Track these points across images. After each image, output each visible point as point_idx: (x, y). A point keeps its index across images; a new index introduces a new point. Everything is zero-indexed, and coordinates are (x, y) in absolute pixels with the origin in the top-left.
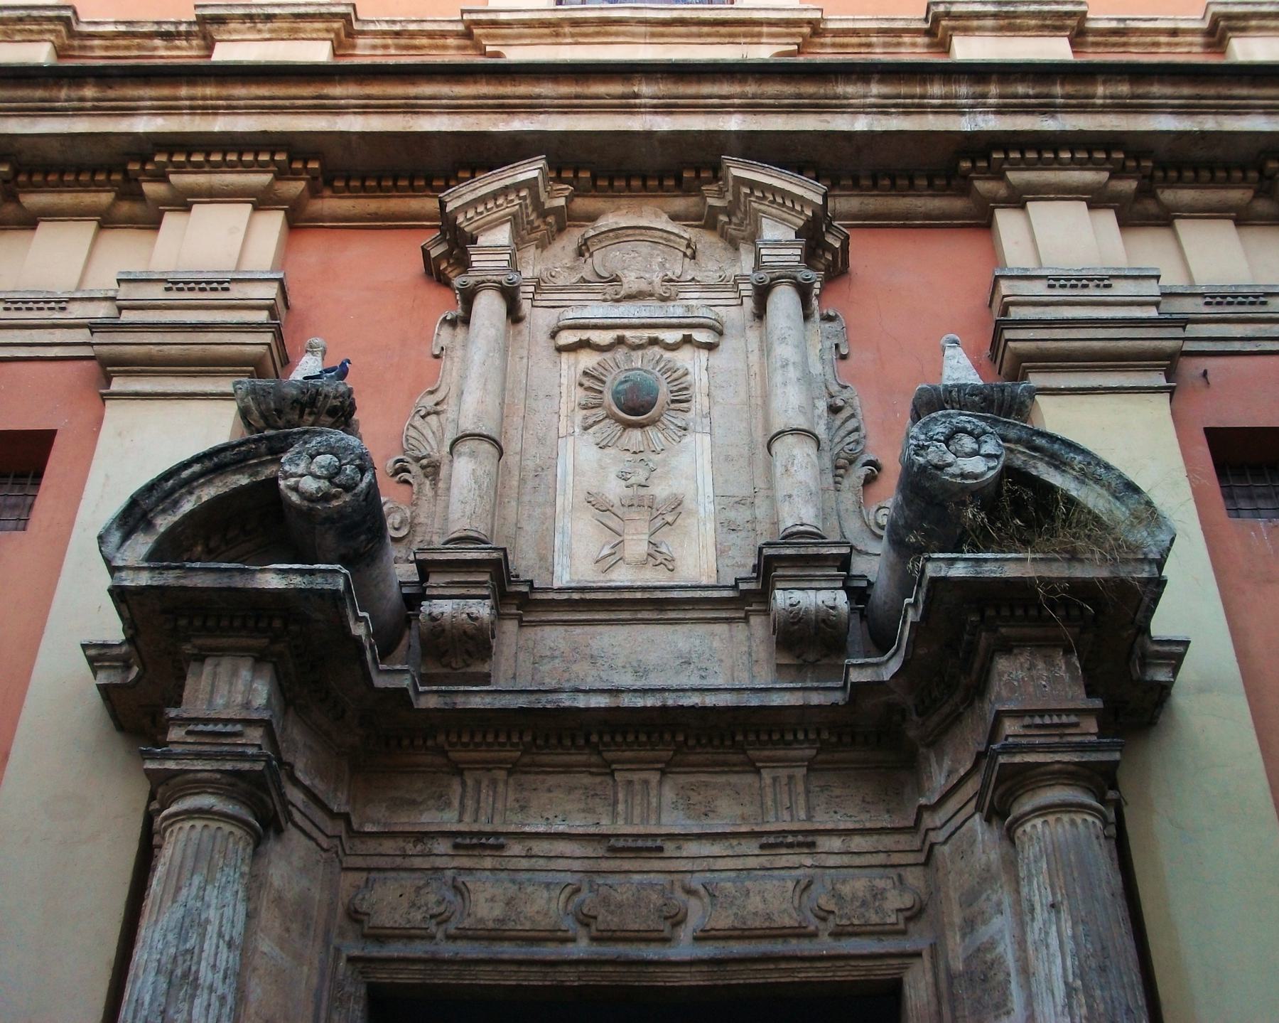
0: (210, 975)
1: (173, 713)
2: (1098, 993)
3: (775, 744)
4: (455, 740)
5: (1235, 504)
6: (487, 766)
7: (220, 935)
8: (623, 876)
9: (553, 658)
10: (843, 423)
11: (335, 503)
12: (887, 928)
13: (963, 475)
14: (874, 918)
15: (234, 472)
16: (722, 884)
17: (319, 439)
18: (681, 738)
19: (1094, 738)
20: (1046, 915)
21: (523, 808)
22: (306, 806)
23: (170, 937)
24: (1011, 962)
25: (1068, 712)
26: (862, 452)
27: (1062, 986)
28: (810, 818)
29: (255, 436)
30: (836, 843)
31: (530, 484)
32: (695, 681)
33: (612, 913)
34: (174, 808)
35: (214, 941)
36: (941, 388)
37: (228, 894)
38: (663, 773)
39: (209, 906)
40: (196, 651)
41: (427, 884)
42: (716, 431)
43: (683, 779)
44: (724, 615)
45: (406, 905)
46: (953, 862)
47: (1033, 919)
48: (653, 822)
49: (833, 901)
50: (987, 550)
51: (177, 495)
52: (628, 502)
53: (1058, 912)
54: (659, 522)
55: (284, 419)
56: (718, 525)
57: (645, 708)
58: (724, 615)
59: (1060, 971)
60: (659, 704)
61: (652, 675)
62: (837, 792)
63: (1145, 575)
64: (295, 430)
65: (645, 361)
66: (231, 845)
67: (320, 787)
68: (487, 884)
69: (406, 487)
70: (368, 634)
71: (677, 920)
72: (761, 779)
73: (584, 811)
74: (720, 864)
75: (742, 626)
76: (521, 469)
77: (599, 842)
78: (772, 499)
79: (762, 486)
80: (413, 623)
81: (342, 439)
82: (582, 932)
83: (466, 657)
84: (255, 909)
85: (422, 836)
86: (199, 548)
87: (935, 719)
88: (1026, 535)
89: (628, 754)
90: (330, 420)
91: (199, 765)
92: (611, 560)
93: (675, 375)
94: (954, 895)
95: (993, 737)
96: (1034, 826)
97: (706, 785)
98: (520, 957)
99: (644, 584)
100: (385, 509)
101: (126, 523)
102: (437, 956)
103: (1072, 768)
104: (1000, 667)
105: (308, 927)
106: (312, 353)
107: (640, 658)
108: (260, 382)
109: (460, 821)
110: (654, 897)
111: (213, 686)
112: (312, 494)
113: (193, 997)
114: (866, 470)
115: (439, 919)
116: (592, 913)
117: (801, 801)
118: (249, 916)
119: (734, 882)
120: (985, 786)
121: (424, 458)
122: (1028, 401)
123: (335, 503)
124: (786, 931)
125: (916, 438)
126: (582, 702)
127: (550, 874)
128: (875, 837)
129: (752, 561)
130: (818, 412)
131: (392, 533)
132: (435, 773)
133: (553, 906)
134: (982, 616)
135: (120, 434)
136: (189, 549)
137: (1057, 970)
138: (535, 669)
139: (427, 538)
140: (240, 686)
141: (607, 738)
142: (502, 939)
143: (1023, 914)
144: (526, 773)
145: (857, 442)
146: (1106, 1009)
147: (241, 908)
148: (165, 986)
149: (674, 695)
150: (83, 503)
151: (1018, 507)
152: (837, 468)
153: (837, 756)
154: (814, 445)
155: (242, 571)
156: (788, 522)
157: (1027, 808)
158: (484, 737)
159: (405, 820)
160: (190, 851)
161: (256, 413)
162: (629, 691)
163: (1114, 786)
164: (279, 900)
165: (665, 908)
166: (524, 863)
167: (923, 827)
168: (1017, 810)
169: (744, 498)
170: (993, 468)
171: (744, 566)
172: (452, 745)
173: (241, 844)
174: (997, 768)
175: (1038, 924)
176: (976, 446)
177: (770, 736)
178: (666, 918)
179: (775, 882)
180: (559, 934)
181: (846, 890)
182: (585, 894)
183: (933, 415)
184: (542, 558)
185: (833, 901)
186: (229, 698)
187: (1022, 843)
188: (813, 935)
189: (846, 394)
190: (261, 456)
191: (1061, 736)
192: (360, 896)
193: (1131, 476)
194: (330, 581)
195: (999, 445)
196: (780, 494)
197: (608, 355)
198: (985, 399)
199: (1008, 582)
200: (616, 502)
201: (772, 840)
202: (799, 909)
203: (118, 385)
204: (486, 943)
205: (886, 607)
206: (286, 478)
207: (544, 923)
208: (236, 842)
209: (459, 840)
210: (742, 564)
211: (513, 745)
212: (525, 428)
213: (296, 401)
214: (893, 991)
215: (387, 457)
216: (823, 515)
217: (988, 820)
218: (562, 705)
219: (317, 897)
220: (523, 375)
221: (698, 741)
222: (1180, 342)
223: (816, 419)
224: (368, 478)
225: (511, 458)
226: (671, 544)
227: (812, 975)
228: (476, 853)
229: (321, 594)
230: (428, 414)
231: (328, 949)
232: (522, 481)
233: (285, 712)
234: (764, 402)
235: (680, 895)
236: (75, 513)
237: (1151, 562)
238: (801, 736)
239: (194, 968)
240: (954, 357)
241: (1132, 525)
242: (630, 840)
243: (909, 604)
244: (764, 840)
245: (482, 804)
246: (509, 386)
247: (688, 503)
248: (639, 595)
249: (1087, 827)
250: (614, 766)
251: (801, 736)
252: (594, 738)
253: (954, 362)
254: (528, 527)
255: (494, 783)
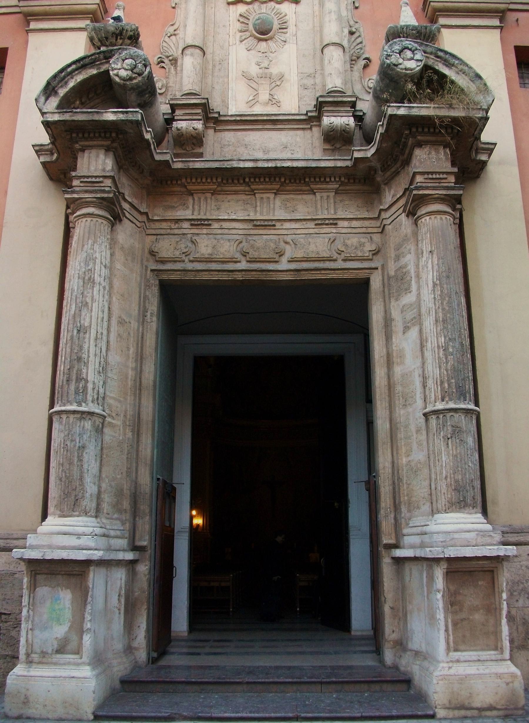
0: (99, 279)
1: (73, 174)
2: (445, 286)
3: (322, 183)
4: (189, 181)
5: (524, 81)
6: (203, 191)
7: (101, 263)
8: (259, 236)
9: (229, 145)
10: (355, 40)
11: (135, 81)
12: (365, 258)
13: (406, 69)
14: (360, 254)
15: (90, 68)
16: (299, 240)
17: (126, 52)
18: (283, 180)
19: (453, 185)
20: (428, 255)
21: (218, 209)
22: (131, 210)
23: (82, 264)
24: (413, 274)
25: (443, 173)
26: (363, 53)
27: (432, 283)
28: (335, 213)
29: (98, 51)
30: (346, 224)
31: (217, 68)
32: (289, 155)
33: (255, 251)
34: (78, 213)
35: (99, 265)
36: (399, 26)
37: (103, 247)
38: (276, 194)
39: (96, 252)
40: (81, 147)
41: (181, 240)
42: (299, 43)
43: (284, 197)
44: (301, 126)
45: (172, 249)
46: (392, 232)
47: (422, 257)
48: (271, 214)
49: (344, 247)
50: (415, 102)
51: (66, 79)
52: (260, 76)
53: (433, 254)
54: (274, 85)
55: (109, 41)
56: (299, 86)
57: (268, 168)
58: (301, 126)
59: (431, 277)
60: (274, 166)
61: (271, 153)
62: (347, 202)
63: (480, 115)
64: (115, 48)
65: (267, 9)
66: (102, 228)
67: (135, 202)
68: (205, 240)
69: (163, 69)
70: (152, 138)
71: (281, 254)
72: (316, 197)
73: (243, 210)
74: (299, 232)
75: (309, 131)
76: (213, 60)
77: (250, 222)
78: (323, 75)
79: (319, 68)
80: (170, 131)
81: (136, 52)
82: (243, 259)
83: (193, 146)
84: (114, 252)
85: (177, 221)
86: (78, 102)
87: (389, 173)
88: (432, 95)
89: (261, 186)
90: (129, 42)
91: (87, 195)
92: (253, 102)
93: (281, 16)
94: (392, 246)
95: (411, 183)
96: (426, 220)
97: (293, 199)
98: (219, 269)
99: (268, 113)
100: (155, 79)
101: (46, 93)
102: (186, 269)
103: (442, 196)
104: (416, 153)
105: (134, 258)
106: (119, 9)
107: (266, 145)
108: (97, 25)
109: (193, 214)
110: (272, 245)
111: (89, 162)
112: (124, 78)
113: (93, 287)
114: (364, 62)
115: (186, 254)
116: (247, 251)
117: (332, 206)
118: (112, 255)
119: (304, 239)
120: (407, 202)
121: (170, 56)
122: (437, 34)
123: (135, 81)
124: (325, 258)
125: (386, 51)
126: (242, 165)
127: (230, 235)
128: (362, 221)
129: (314, 103)
130: (344, 34)
131: (159, 91)
132: (182, 195)
133: (232, 248)
134: (410, 131)
135: (36, 49)
136: (74, 103)
137: (430, 277)
138: (221, 150)
139: (174, 93)
140: (100, 162)
141: (252, 180)
142: (211, 262)
143: (419, 254)
144: (220, 194)
145: (361, 49)
146: (448, 292)
147: (108, 253)
148: (82, 283)
149: (280, 162)
150: (24, 81)
151: (430, 82)
152: (352, 60)
153: (348, 188)
154: (342, 50)
155: (97, 112)
156: (330, 86)
157: (423, 212)
158: (202, 179)
159: (171, 214)
160: (87, 230)
161: (96, 39)
162: (261, 160)
163: (460, 203)
164: (122, 248)
165: (276, 249)
166: (219, 231)
167: (381, 218)
168: (419, 213)
169: (311, 74)
170: (419, 66)
171: (310, 105)
172: (188, 183)
173: (106, 227)
174: (412, 195)
175: (424, 259)
176: (412, 56)
177: (320, 179)
178: (277, 253)
179: (321, 239)
180: (234, 259)
181: (349, 242)
182: (244, 244)
183: (395, 40)
184: (223, 101)
185: (344, 247)
186: (96, 167)
187: (421, 226)
188: (335, 260)
189: (357, 26)
190: (101, 60)
191: (439, 183)
192: (154, 245)
193: (479, 71)
194: (135, 116)
195: (422, 55)
196: (326, 73)
197: (250, 6)
198: (418, 32)
199: (423, 117)
200: (255, 76)
201: (320, 222)
202: (330, 250)
203: (33, 25)
204: (205, 263)
205: (371, 124)
206: (113, 70)
207: (228, 255)
208: (105, 226)
209: (193, 222)
210: (309, 105)
211: (213, 183)
212: (214, 41)
213: (113, 33)
214: (366, 283)
215: (154, 56)
216: (345, 83)
217: (407, 216)
218: (234, 166)
219: (137, 246)
220: (213, 16)
221: (290, 181)
222: (507, 5)
223: (343, 37)
224: (148, 69)
225: (209, 56)
226: (279, 95)
227: (335, 276)
228: (200, 227)
229: (131, 122)
230: (171, 35)
231: (143, 267)
232: (214, 66)
233: (119, 172)
234: (320, 30)
235: (282, 244)
236: (21, 86)
237: (483, 110)
238: (333, 179)
239: (92, 277)
240: (406, 11)
241: (477, 93)
242: (262, 221)
243: (380, 125)
244: (317, 222)
245: (202, 208)
246: (206, 21)
247: (286, 76)
248: (265, 118)
249: (447, 221)
250: (255, 191)
251: (333, 179)
252: (247, 180)
253: (405, 14)
254: (217, 87)
255: (206, 198)
